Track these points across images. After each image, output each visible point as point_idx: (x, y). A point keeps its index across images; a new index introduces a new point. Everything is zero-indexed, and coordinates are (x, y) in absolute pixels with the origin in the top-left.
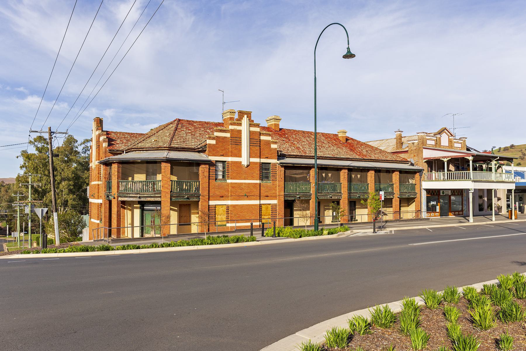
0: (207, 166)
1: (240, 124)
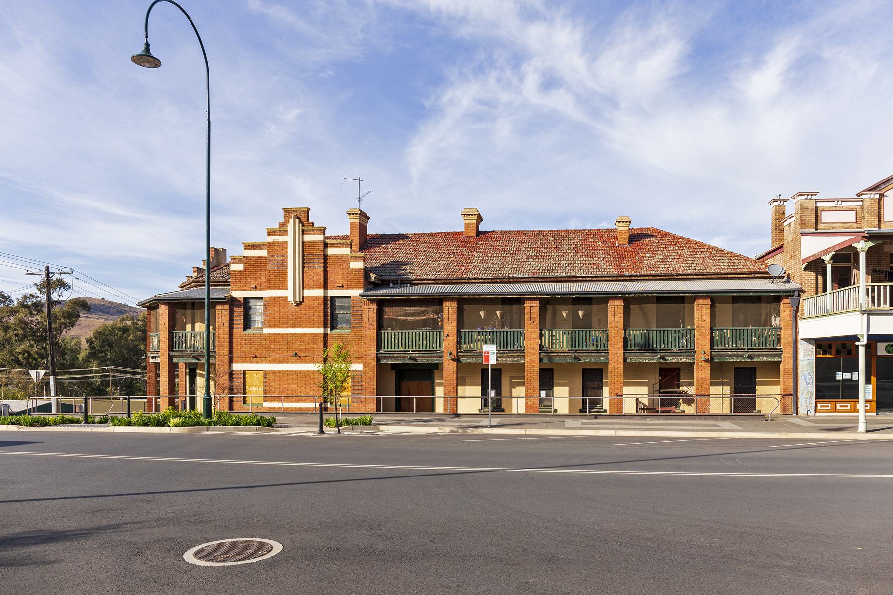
0: (227, 307)
1: (285, 232)
